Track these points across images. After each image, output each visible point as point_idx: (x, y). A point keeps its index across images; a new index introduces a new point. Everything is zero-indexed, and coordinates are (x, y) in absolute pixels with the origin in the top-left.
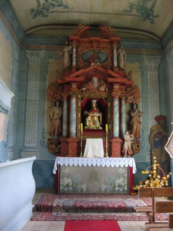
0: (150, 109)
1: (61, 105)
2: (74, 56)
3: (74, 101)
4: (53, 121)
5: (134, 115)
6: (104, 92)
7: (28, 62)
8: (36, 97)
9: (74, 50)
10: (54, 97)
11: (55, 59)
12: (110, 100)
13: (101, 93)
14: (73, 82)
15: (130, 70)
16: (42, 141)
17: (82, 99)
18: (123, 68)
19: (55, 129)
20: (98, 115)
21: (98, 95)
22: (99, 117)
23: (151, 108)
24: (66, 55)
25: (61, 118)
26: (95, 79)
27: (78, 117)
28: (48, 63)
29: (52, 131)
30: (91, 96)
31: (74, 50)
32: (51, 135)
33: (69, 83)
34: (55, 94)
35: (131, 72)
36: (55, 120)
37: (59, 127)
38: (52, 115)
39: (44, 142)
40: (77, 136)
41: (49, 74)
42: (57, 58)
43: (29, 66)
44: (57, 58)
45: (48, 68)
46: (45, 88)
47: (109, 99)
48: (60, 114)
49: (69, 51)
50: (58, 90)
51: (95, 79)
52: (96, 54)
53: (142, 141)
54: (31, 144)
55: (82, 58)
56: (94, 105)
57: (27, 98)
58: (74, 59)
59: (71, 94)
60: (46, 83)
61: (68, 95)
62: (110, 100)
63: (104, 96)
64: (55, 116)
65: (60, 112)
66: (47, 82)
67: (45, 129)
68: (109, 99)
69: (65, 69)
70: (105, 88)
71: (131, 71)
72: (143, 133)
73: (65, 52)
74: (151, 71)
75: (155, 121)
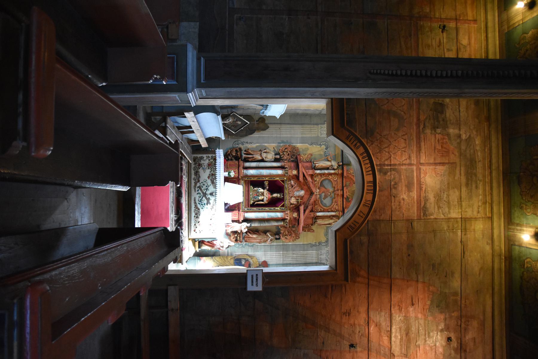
0: (276, 254)
1: (276, 160)
2: (326, 172)
3: (280, 172)
4: (259, 153)
5: (268, 236)
6: (290, 203)
7: (321, 124)
8: (289, 134)
9: (332, 171)
10: (285, 153)
11: (325, 152)
12: (282, 209)
13: (289, 199)
14: (299, 171)
15: (315, 231)
16: (239, 141)
17: (283, 181)
18: (317, 223)
19: (252, 155)
20: (265, 199)
21: (287, 197)
22: (262, 200)
23: (277, 254)
24: (328, 164)
25: (262, 161)
26: (302, 193)
27: (264, 177)
28: (320, 145)
29: (250, 151)
30: (286, 190)
31: (332, 171)
32: (245, 151)
33: (297, 168)
34: (287, 154)
35: (313, 231)
36: (261, 154)
37: (254, 158)
38: (265, 151)
39: (238, 144)
40: (245, 177)
41: (309, 146)
42: (326, 153)
43: (316, 126)
44: (327, 154)
45: (315, 145)
46: (293, 143)
47: (283, 209)
48: (267, 160)
49: (332, 166)
50: (291, 157)
51: (302, 193)
52: (329, 194)
53: (242, 245)
54: (362, 156)
55: (325, 180)
56: (275, 195)
57: (282, 125)
58: (323, 171)
59: (287, 169)
60: (300, 143)
61: (286, 166)
62: (282, 209)
63: (287, 203)
64: (265, 154)
65: (269, 160)
66: (301, 144)
67: (252, 145)
68: (283, 208)
69: (313, 163)
70: (293, 204)
71: (314, 232)
72: (250, 246)
73: (331, 162)
74: (316, 254)
75: (263, 261)
